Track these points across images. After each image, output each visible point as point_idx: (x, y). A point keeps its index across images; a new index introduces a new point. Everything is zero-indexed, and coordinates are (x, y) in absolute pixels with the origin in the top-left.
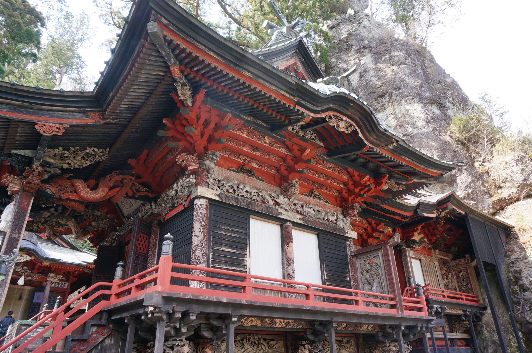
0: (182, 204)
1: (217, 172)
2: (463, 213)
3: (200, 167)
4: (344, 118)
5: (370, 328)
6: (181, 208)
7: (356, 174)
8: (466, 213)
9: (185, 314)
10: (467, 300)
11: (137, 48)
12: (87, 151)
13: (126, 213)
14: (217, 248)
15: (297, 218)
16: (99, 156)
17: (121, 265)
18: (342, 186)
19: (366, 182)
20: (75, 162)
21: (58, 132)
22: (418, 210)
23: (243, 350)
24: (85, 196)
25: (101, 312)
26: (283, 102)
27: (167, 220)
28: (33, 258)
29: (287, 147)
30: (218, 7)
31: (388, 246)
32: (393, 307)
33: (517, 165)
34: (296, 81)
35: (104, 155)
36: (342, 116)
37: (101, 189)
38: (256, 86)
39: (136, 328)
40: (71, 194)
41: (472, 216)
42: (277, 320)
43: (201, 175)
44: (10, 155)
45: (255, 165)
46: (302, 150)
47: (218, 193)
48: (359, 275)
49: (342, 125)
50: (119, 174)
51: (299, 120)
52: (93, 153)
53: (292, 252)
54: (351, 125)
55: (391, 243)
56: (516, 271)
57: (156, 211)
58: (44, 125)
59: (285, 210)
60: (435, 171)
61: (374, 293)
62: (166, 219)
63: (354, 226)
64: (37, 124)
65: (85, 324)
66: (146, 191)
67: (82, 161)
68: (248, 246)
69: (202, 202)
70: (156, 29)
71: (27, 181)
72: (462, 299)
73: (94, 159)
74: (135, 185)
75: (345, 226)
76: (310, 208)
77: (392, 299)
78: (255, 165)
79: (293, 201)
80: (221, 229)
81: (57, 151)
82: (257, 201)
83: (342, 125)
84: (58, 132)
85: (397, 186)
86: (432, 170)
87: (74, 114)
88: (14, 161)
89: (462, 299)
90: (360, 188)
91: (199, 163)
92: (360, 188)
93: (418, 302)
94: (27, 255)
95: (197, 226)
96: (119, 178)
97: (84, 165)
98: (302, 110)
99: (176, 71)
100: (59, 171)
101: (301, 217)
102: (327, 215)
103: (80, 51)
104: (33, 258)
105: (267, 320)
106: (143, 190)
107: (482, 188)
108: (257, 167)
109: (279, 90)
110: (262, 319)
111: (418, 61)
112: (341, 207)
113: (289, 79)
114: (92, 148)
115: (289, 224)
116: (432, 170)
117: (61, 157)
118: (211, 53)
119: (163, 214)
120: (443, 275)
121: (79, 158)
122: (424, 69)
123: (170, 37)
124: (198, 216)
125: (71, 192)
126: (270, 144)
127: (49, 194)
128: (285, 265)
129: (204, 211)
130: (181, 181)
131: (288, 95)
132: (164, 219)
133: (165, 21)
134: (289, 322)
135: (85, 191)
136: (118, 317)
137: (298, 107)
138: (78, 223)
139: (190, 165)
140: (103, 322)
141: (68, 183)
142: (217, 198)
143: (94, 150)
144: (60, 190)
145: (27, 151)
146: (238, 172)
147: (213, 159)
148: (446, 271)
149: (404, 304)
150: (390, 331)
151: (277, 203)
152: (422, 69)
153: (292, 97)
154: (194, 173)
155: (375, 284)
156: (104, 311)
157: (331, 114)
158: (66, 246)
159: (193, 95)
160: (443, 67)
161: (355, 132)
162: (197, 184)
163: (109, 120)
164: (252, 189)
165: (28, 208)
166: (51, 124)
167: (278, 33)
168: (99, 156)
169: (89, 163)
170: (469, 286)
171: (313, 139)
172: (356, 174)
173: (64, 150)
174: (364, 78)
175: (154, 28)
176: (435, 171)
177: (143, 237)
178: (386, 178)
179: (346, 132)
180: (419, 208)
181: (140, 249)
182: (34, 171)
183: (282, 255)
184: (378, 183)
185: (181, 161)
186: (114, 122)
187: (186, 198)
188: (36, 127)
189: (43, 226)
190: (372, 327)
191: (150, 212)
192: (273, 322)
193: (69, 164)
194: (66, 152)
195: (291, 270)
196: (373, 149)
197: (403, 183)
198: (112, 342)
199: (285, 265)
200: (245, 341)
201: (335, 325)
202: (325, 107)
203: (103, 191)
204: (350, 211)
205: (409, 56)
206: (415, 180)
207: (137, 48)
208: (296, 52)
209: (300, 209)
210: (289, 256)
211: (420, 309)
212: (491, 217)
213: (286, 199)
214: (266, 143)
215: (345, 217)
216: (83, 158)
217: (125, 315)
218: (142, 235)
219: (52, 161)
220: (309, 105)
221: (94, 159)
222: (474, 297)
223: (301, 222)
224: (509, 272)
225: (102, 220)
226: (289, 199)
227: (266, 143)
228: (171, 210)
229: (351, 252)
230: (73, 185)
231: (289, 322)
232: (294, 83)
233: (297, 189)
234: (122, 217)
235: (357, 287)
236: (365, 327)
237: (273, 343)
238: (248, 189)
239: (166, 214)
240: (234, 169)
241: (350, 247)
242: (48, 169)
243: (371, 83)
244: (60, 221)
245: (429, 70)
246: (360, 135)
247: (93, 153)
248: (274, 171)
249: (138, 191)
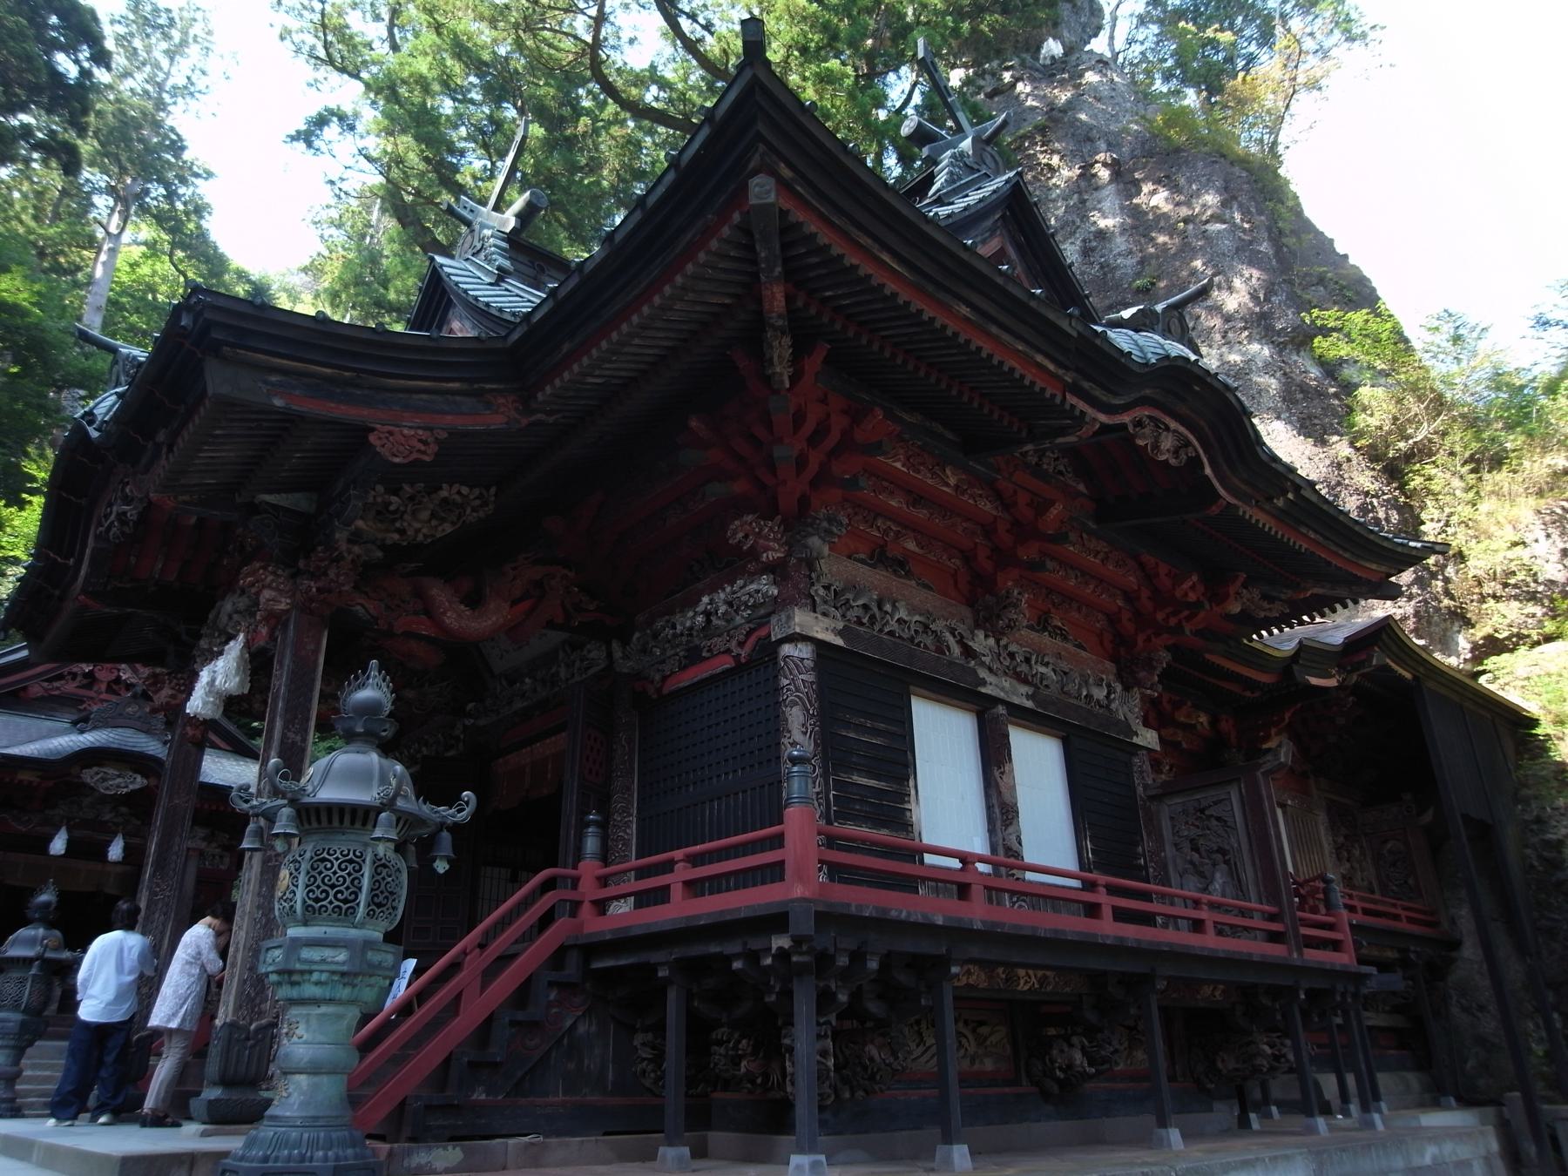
0: (728, 651)
1: (834, 568)
2: (1408, 675)
3: (789, 554)
4: (1173, 425)
5: (1217, 993)
6: (727, 663)
7: (1163, 569)
8: (1415, 678)
9: (858, 957)
10: (1410, 920)
11: (689, 236)
12: (444, 493)
14: (844, 777)
15: (1020, 696)
16: (474, 510)
17: (595, 823)
18: (1120, 603)
19: (1186, 594)
21: (424, 453)
22: (1295, 667)
23: (921, 1049)
24: (455, 625)
26: (1039, 384)
27: (671, 694)
29: (998, 496)
30: (657, 20)
31: (1259, 773)
32: (1274, 937)
33: (1548, 536)
34: (1080, 328)
35: (485, 504)
36: (1168, 420)
38: (980, 344)
41: (1430, 684)
42: (1022, 972)
43: (796, 580)
44: (253, 509)
45: (911, 545)
46: (1042, 507)
47: (840, 625)
48: (1169, 851)
49: (1167, 443)
51: (1063, 431)
52: (458, 498)
53: (1014, 787)
54: (1188, 444)
55: (1268, 766)
56: (1548, 844)
57: (625, 667)
58: (391, 433)
59: (990, 670)
60: (1374, 567)
61: (1216, 898)
62: (665, 691)
63: (1155, 716)
64: (373, 430)
65: (528, 982)
67: (434, 523)
68: (911, 771)
69: (803, 651)
70: (773, 195)
71: (320, 584)
72: (1396, 917)
75: (1129, 715)
76: (1046, 665)
77: (1272, 918)
78: (911, 545)
79: (1006, 647)
80: (848, 725)
82: (926, 647)
83: (1168, 443)
84: (424, 453)
85: (1266, 605)
86: (1368, 565)
87: (458, 398)
89: (1396, 917)
90: (1169, 610)
91: (786, 543)
92: (1169, 610)
93: (1331, 927)
94: (136, 771)
95: (795, 718)
98: (1082, 406)
99: (776, 298)
100: (380, 554)
101: (1030, 690)
102: (1086, 683)
103: (179, 118)
105: (1000, 970)
106: (591, 607)
107: (1446, 602)
108: (917, 550)
109: (1031, 352)
110: (988, 965)
111: (1260, 213)
112: (1114, 659)
113: (1064, 324)
114: (456, 487)
115: (1001, 710)
116: (1368, 565)
117: (379, 513)
118: (886, 257)
119: (658, 677)
120: (1338, 849)
121: (425, 515)
122: (1276, 237)
123: (798, 215)
124: (798, 690)
126: (957, 487)
128: (999, 823)
129: (809, 677)
130: (728, 589)
131: (1051, 367)
132: (659, 691)
133: (786, 173)
134: (1045, 977)
136: (622, 962)
137: (1072, 399)
139: (767, 549)
142: (839, 642)
143: (459, 493)
145: (298, 495)
146: (873, 566)
147: (829, 532)
148: (1346, 837)
149: (1304, 931)
150: (1266, 1001)
151: (968, 652)
152: (1270, 239)
153: (1061, 372)
154: (777, 570)
155: (1218, 875)
157: (1144, 412)
158: (222, 745)
159: (796, 359)
160: (1329, 235)
161: (1195, 462)
162: (779, 605)
163: (539, 416)
164: (909, 609)
165: (317, 659)
166: (406, 431)
167: (953, 156)
168: (474, 510)
169: (448, 528)
170: (1411, 881)
171: (1060, 473)
172: (1163, 569)
174: (1096, 258)
175: (768, 192)
176: (1374, 567)
178: (1238, 583)
179: (1173, 462)
180: (1296, 662)
181: (590, 771)
183: (987, 796)
184: (1218, 598)
185: (740, 535)
186: (551, 420)
187: (742, 638)
188: (372, 438)
190: (1223, 991)
192: (1011, 979)
193: (402, 532)
194: (394, 499)
195: (1014, 838)
196: (1237, 508)
197: (1283, 596)
198: (593, 1028)
199: (999, 823)
200: (924, 1026)
201: (1161, 985)
202: (1134, 396)
204: (1142, 674)
205: (1234, 198)
206: (1317, 590)
207: (689, 236)
208: (1003, 217)
209: (1024, 668)
210: (1007, 797)
211: (1336, 946)
212: (1468, 681)
213: (991, 641)
214: (947, 485)
215: (1127, 688)
216: (433, 515)
217: (656, 957)
220: (1098, 393)
221: (460, 516)
222: (1425, 913)
223: (1029, 704)
224: (1527, 846)
226: (998, 642)
227: (947, 485)
228: (683, 668)
229: (1146, 787)
231: (1045, 977)
232: (1075, 334)
233: (1022, 613)
235: (1166, 882)
236: (1207, 990)
237: (984, 1030)
238: (902, 613)
239: (665, 679)
240: (862, 556)
241: (1142, 772)
243: (1118, 274)
245: (1291, 241)
246: (1208, 471)
247: (458, 498)
248: (958, 562)
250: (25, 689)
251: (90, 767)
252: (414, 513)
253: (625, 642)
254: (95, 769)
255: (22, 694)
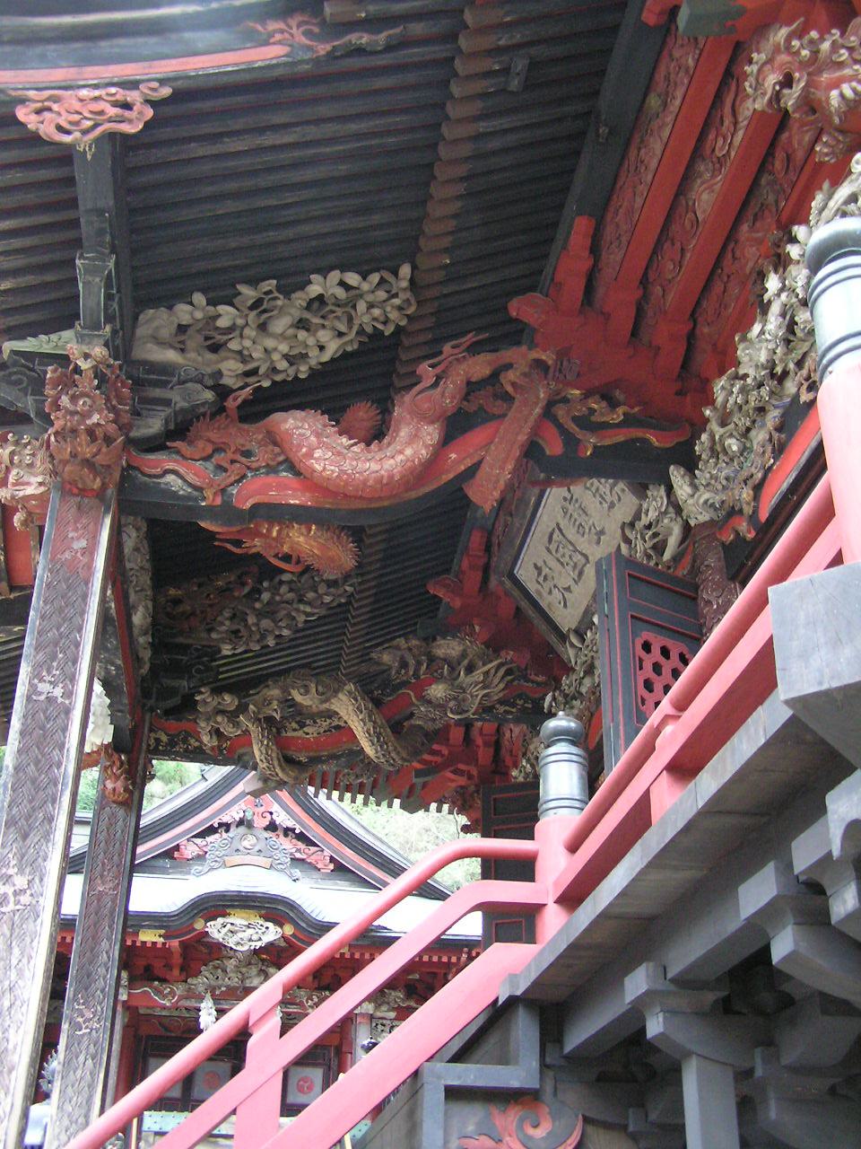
12: (315, 289)
13: (567, 618)
16: (371, 306)
20: (270, 343)
25: (498, 1014)
28: (289, 930)
37: (404, 432)
39: (743, 1075)
40: (271, 478)
50: (474, 349)
52: (341, 293)
66: (628, 421)
73: (350, 320)
74: (565, 400)
81: (183, 312)
88: (19, 382)
94: (267, 920)
96: (480, 367)
97: (315, 358)
104: (289, 930)
114: (335, 276)
125: (272, 469)
127: (174, 495)
135: (328, 447)
138: (377, 703)
140: (520, 1073)
141: (250, 437)
143: (342, 284)
144: (220, 468)
156: (512, 1002)
165: (92, 560)
169: (333, 347)
173: (212, 302)
177: (665, 652)
182: (77, 370)
185: (772, 79)
188: (22, 114)
189: (237, 725)
191: (673, 542)
203: (414, 437)
218: (657, 642)
219: (171, 356)
225: (470, 669)
230: (273, 439)
234: (553, 640)
242: (157, 393)
244: (298, 698)
249: (585, 423)
250: (177, 848)
251: (214, 918)
252: (263, 327)
253: (691, 464)
254: (220, 920)
255: (176, 854)
